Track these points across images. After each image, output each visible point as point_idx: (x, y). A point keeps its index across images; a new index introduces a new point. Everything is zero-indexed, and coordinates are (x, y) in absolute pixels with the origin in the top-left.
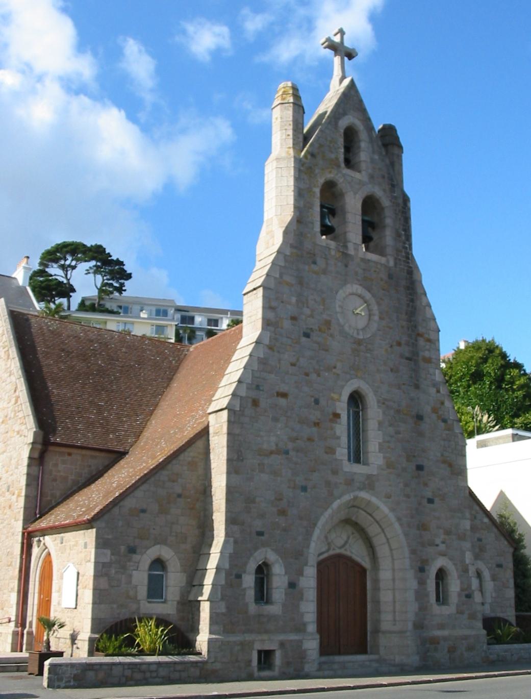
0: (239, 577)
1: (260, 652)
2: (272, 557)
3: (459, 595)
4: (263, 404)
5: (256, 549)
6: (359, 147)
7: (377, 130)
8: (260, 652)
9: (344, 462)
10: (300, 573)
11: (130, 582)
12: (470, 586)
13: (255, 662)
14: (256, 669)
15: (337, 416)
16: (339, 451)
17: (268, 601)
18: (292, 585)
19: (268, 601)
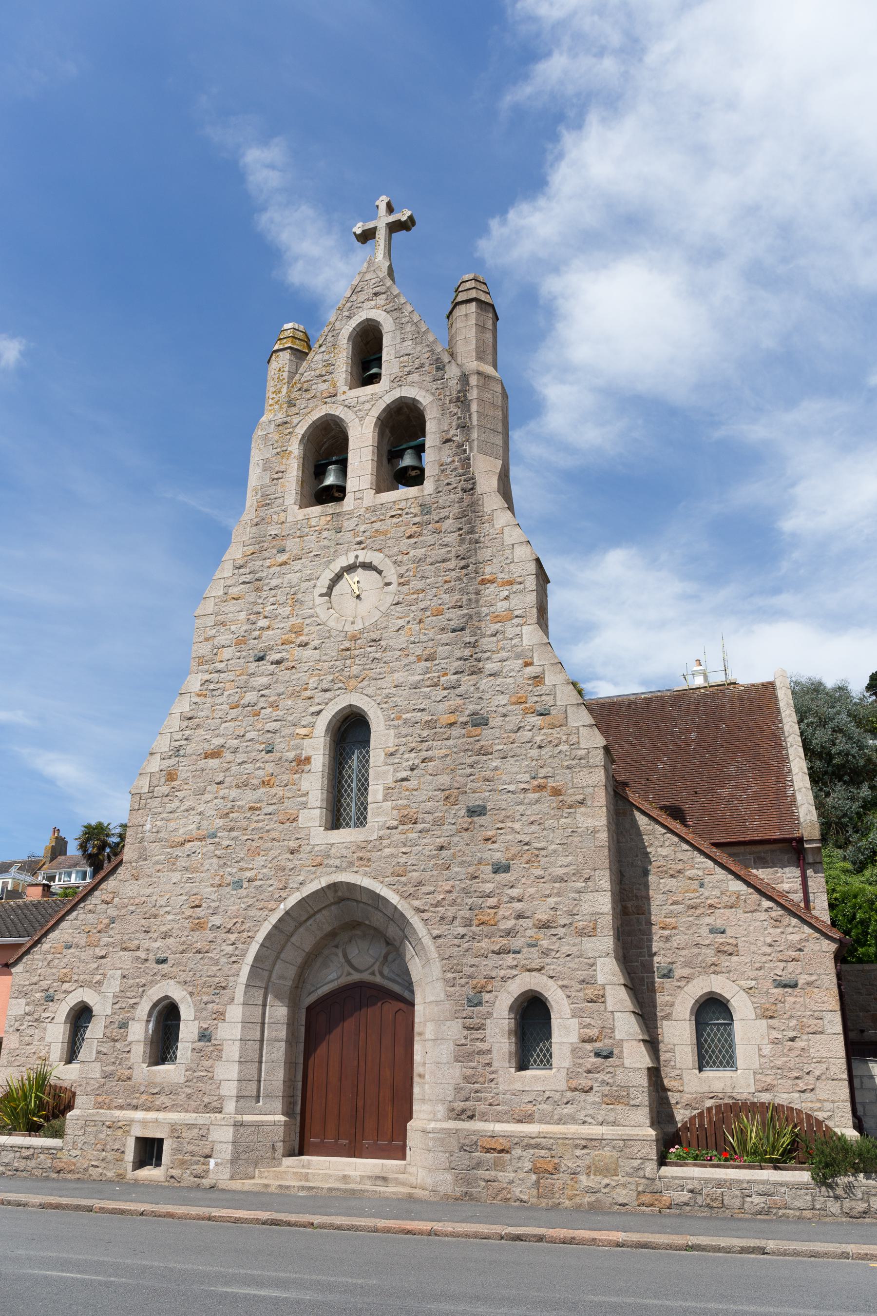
0: (124, 1025)
1: (138, 1139)
2: (178, 994)
3: (574, 1051)
4: (183, 773)
5: (153, 983)
6: (338, 985)
7: (400, 467)
8: (138, 1139)
9: (313, 831)
10: (219, 1016)
11: (42, 1039)
12: (607, 1030)
13: (130, 1155)
14: (130, 1166)
15: (302, 762)
16: (303, 815)
17: (728, 1061)
18: (205, 1036)
19: (728, 1061)
